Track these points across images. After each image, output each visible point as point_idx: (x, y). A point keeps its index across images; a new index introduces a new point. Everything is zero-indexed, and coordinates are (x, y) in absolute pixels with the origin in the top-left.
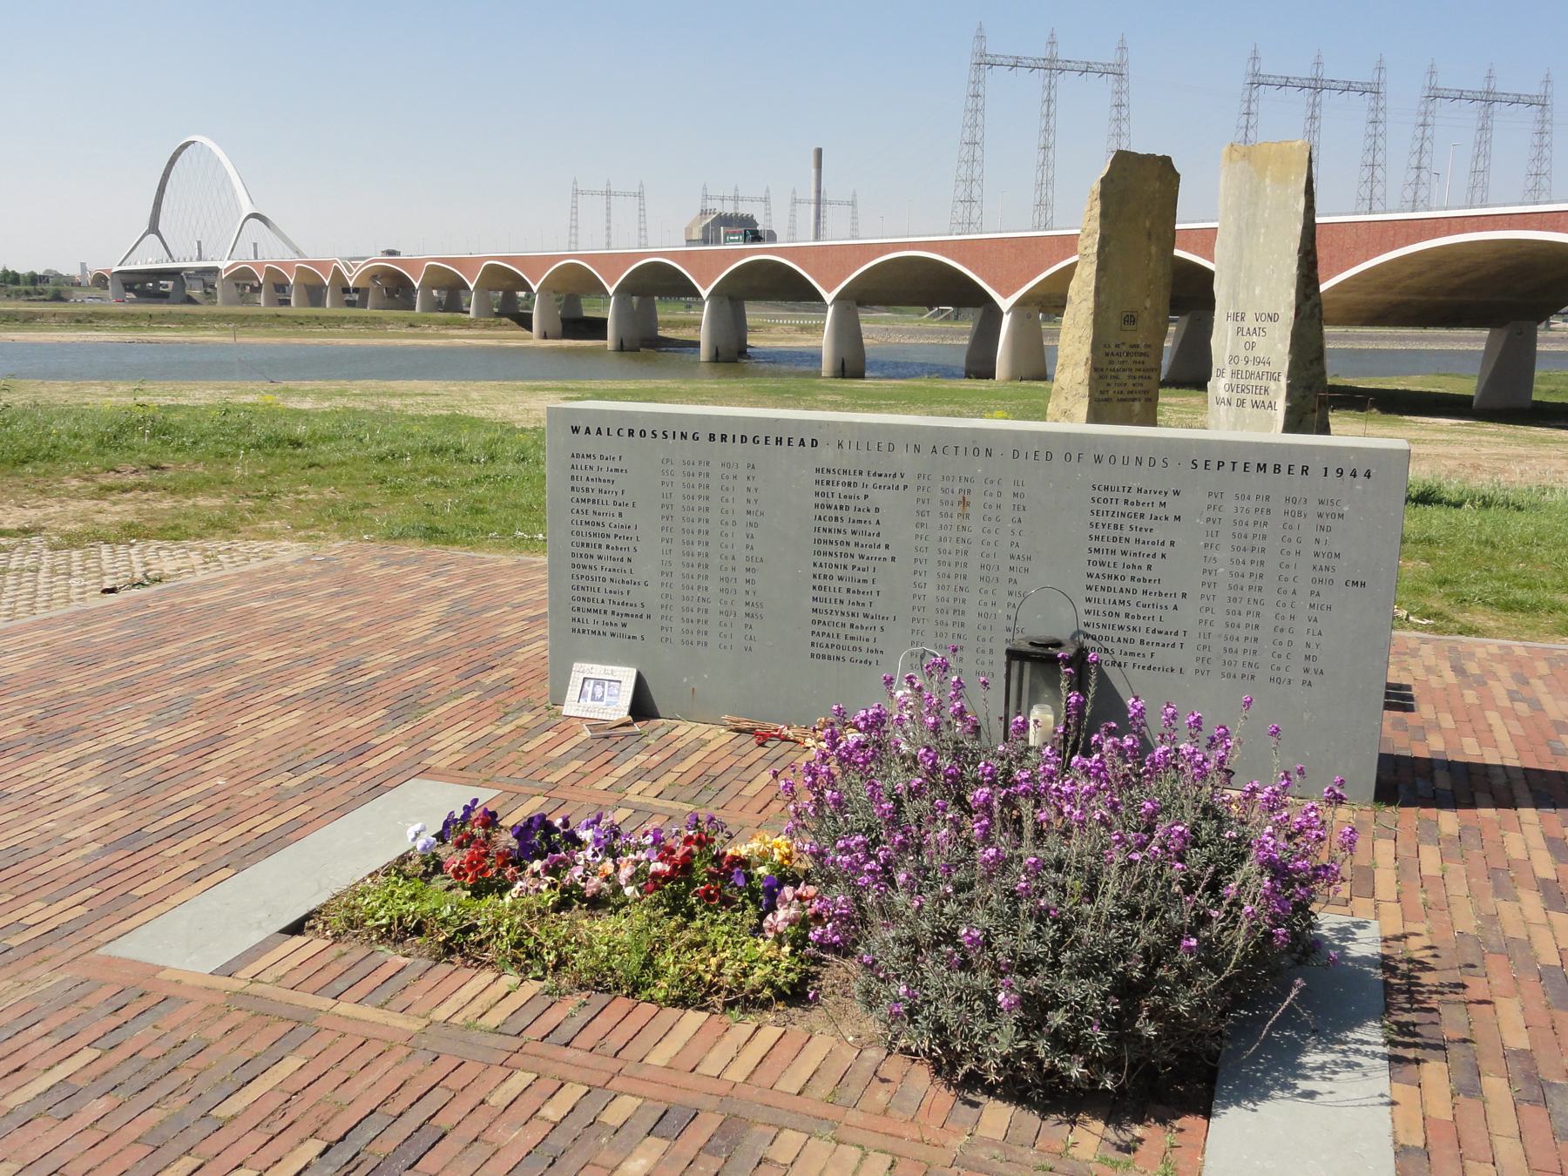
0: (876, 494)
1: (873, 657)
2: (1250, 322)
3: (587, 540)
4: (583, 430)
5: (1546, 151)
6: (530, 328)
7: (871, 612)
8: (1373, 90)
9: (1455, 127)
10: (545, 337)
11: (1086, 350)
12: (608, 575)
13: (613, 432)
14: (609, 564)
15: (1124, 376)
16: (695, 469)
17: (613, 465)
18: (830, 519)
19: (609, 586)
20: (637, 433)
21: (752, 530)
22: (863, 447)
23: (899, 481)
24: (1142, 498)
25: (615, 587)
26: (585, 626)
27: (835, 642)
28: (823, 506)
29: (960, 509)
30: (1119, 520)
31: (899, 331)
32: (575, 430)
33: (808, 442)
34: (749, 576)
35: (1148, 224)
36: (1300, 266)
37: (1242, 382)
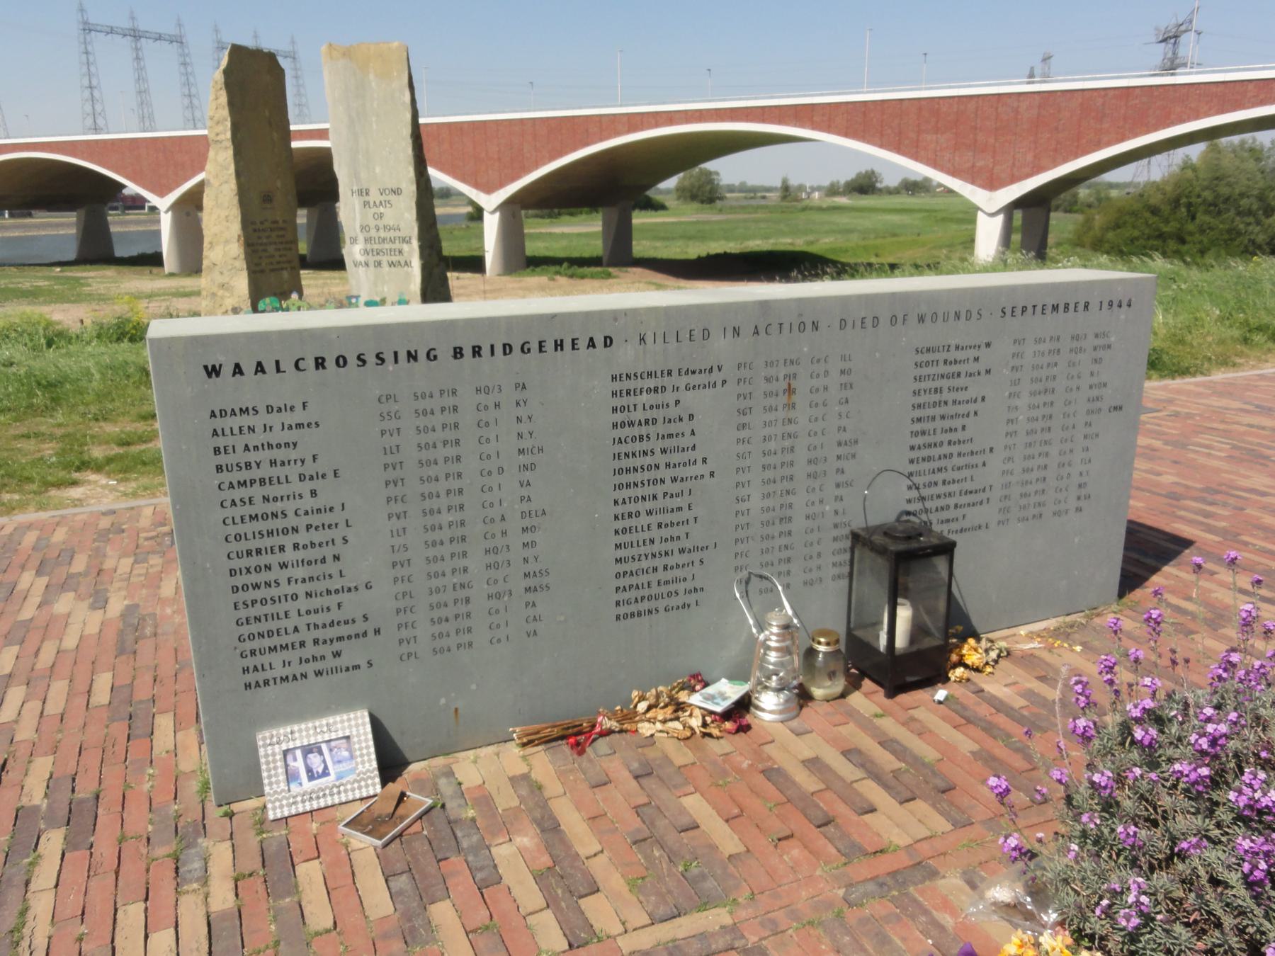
0: (688, 398)
1: (690, 599)
2: (374, 196)
3: (253, 544)
4: (227, 370)
7: (687, 544)
8: (178, 40)
11: (235, 228)
12: (301, 589)
13: (287, 365)
14: (300, 572)
15: (271, 249)
16: (435, 403)
17: (289, 419)
18: (634, 439)
19: (303, 604)
20: (330, 363)
21: (528, 475)
22: (672, 338)
23: (717, 377)
24: (960, 355)
25: (316, 602)
26: (269, 674)
27: (646, 592)
28: (623, 425)
29: (783, 399)
30: (938, 384)
32: (213, 371)
33: (599, 341)
34: (528, 537)
35: (267, 113)
37: (375, 247)
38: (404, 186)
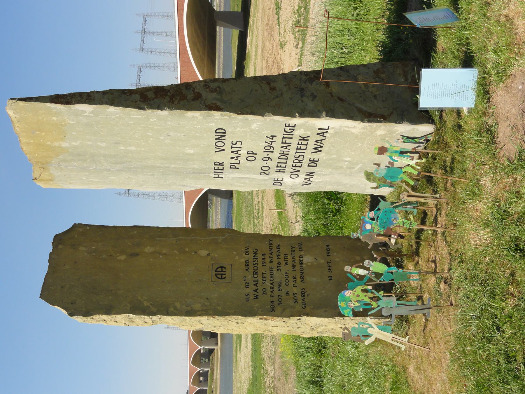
5: (161, 14)
6: (214, 349)
8: (140, 68)
9: (151, 42)
10: (217, 344)
15: (278, 276)
31: (216, 220)
35: (123, 257)
36: (160, 107)
37: (290, 163)
38: (214, 126)
